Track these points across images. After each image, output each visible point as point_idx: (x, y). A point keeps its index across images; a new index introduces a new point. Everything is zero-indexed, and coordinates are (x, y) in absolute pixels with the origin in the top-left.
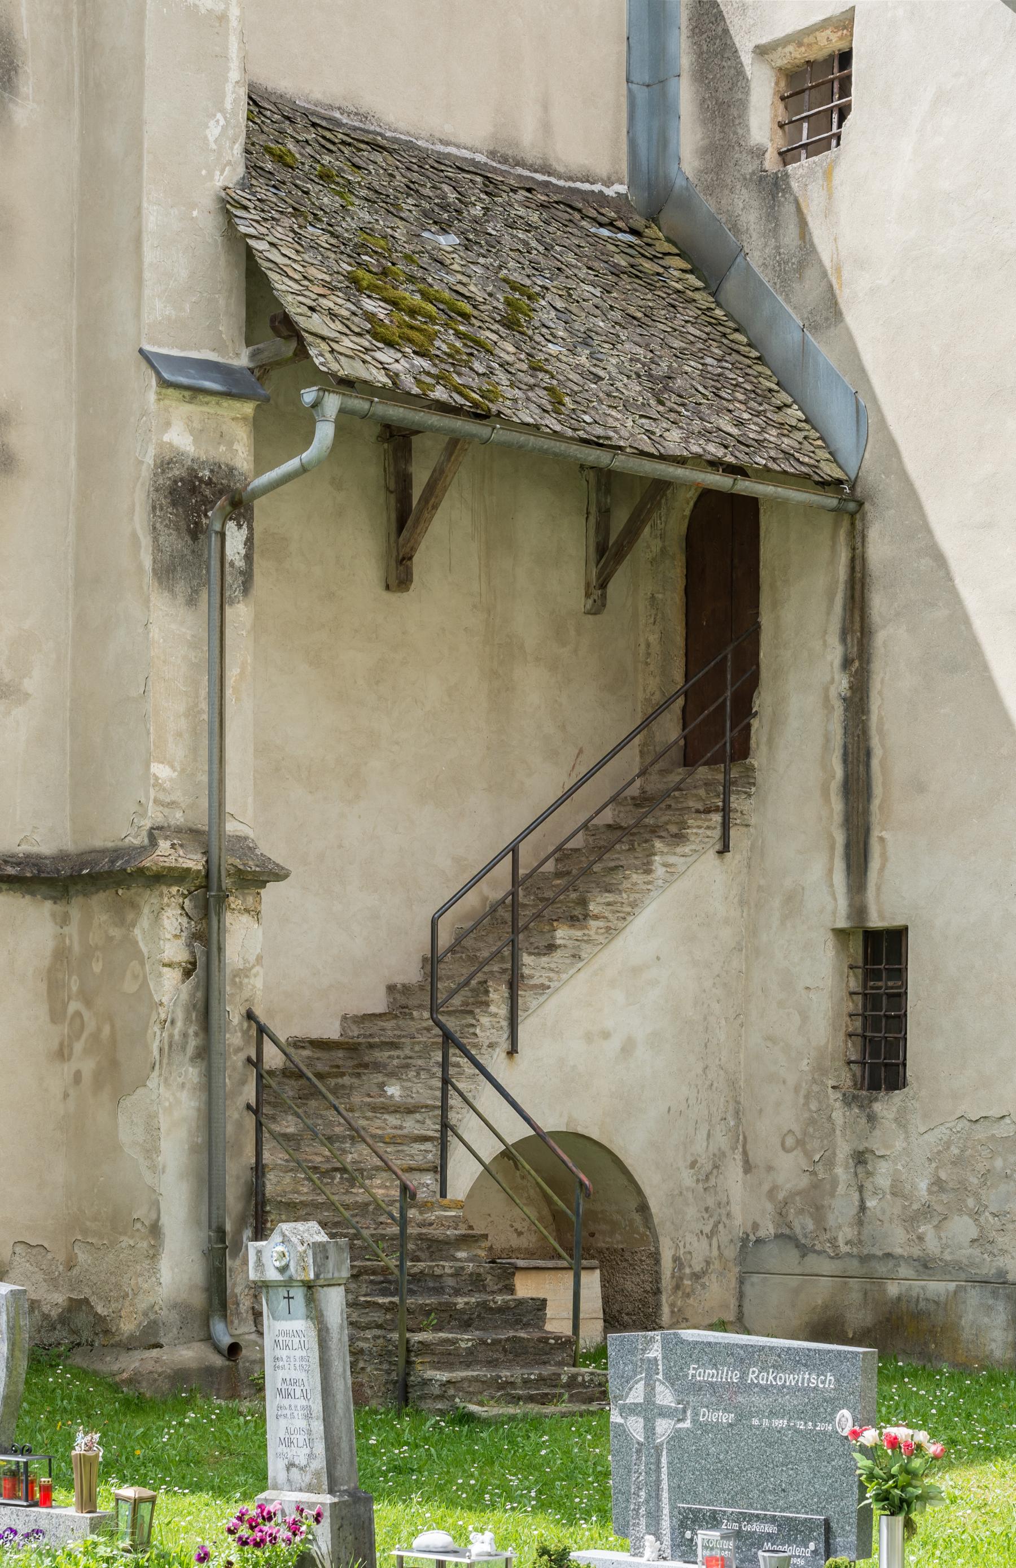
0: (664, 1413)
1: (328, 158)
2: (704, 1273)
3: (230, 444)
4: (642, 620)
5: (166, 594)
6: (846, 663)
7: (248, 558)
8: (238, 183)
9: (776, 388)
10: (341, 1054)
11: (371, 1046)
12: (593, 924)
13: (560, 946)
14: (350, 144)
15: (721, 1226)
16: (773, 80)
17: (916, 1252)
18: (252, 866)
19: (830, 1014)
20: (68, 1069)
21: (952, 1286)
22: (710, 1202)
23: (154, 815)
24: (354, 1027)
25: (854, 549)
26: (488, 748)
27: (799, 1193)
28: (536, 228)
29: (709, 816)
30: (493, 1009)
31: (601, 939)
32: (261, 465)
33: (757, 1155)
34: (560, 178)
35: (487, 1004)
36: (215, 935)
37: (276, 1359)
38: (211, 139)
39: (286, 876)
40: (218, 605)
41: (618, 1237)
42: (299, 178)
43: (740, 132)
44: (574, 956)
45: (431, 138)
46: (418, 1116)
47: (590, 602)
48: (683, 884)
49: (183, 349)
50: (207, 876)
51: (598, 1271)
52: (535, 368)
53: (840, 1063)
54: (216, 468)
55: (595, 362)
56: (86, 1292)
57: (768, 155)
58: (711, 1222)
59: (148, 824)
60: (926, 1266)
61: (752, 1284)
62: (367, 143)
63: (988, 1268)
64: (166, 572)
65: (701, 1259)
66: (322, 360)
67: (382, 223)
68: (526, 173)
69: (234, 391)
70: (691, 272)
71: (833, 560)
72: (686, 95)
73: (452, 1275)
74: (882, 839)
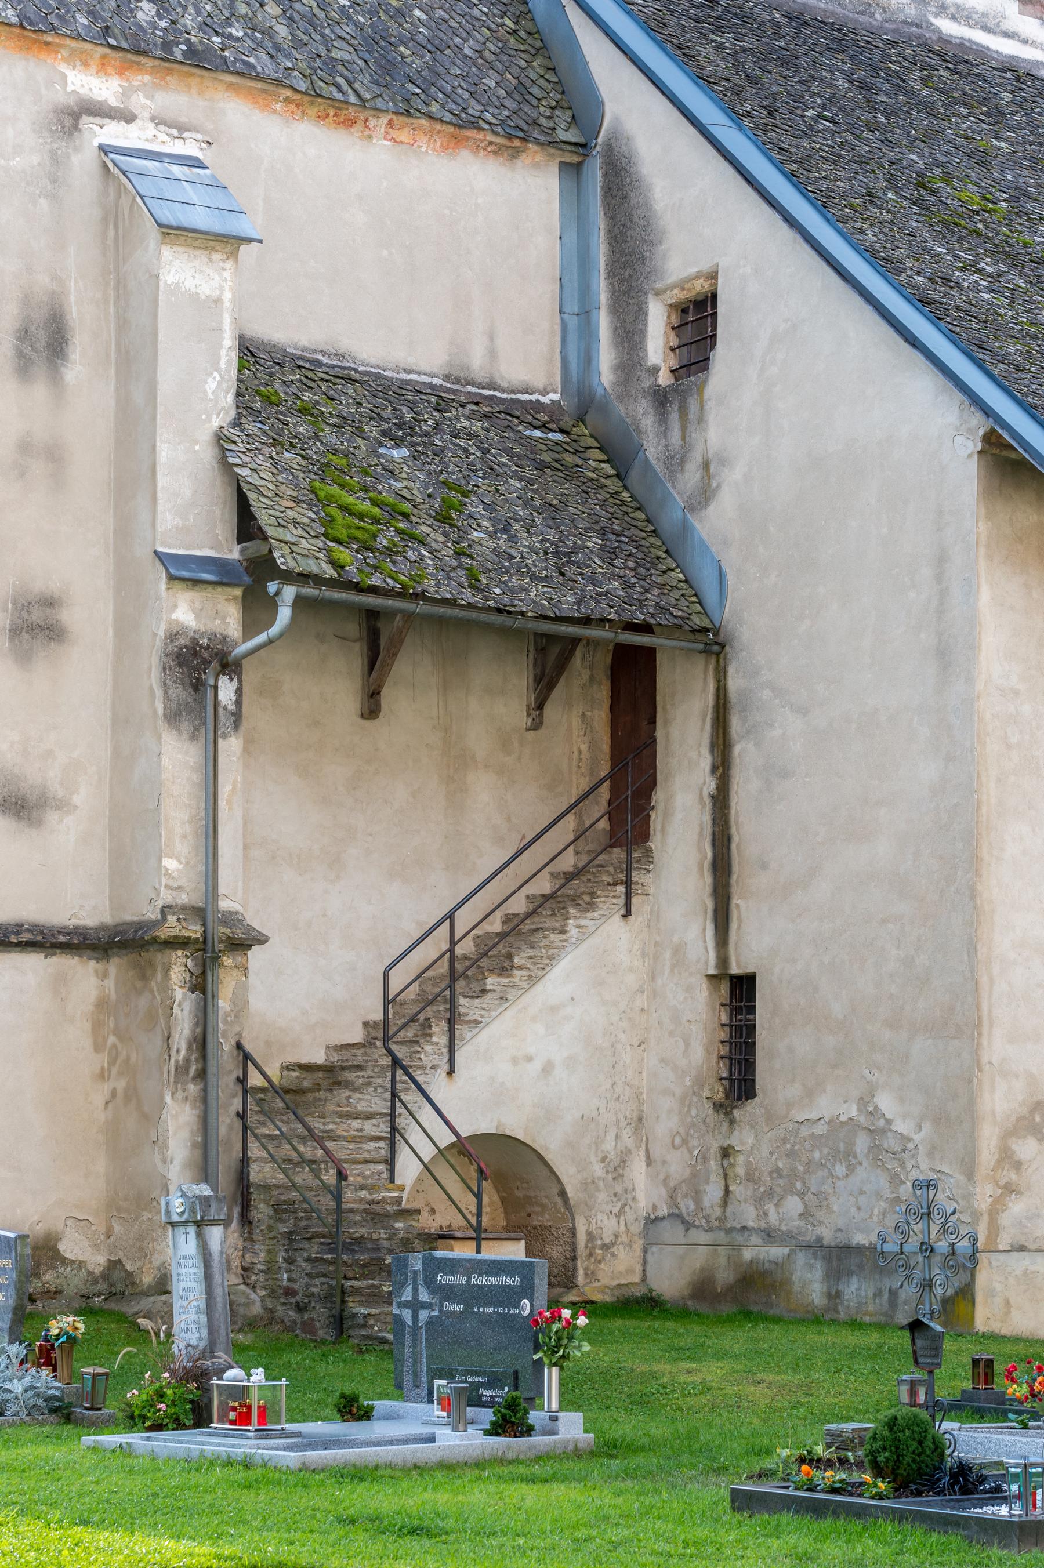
0: (424, 1306)
1: (307, 394)
2: (613, 1244)
3: (224, 619)
4: (575, 733)
5: (174, 732)
6: (714, 769)
7: (239, 703)
8: (230, 423)
9: (664, 555)
10: (321, 1074)
11: (343, 1068)
12: (517, 973)
13: (490, 991)
14: (327, 381)
15: (627, 1208)
16: (666, 314)
18: (239, 934)
19: (705, 1040)
20: (106, 1088)
21: (787, 1250)
22: (618, 1189)
23: (166, 897)
24: (335, 1055)
25: (718, 681)
26: (446, 837)
27: (684, 1181)
28: (477, 436)
29: (614, 888)
30: (435, 1039)
31: (525, 985)
33: (657, 1152)
34: (503, 391)
35: (430, 1035)
36: (210, 986)
37: (179, 1275)
38: (210, 392)
39: (266, 941)
40: (212, 740)
41: (547, 1216)
42: (281, 413)
43: (641, 354)
44: (501, 998)
45: (397, 369)
46: (374, 1121)
47: (530, 720)
49: (188, 549)
50: (205, 942)
51: (523, 1242)
52: (459, 554)
53: (713, 1080)
55: (510, 544)
56: (120, 1255)
57: (661, 373)
58: (619, 1204)
59: (160, 903)
60: (769, 1235)
61: (653, 1253)
62: (342, 378)
64: (173, 717)
65: (610, 1233)
66: (283, 560)
68: (476, 390)
69: (225, 580)
70: (607, 461)
71: (704, 690)
73: (386, 1239)
74: (738, 906)
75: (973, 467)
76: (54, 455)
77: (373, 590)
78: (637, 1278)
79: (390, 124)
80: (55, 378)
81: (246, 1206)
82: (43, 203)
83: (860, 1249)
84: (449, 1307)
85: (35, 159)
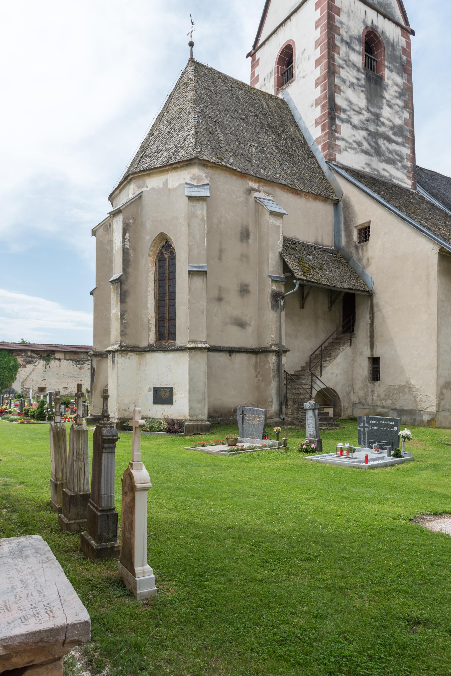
0: (366, 427)
6: (370, 318)
17: (382, 405)
32: (286, 291)
33: (355, 391)
45: (306, 242)
48: (345, 351)
54: (279, 292)
59: (270, 344)
60: (383, 407)
63: (394, 407)
67: (301, 255)
72: (343, 234)
75: (437, 256)
76: (247, 257)
77: (312, 282)
78: (351, 414)
79: (305, 195)
80: (247, 242)
81: (286, 402)
82: (245, 207)
83: (406, 410)
84: (373, 428)
85: (243, 199)
